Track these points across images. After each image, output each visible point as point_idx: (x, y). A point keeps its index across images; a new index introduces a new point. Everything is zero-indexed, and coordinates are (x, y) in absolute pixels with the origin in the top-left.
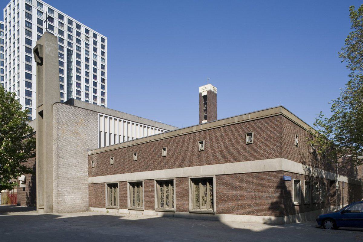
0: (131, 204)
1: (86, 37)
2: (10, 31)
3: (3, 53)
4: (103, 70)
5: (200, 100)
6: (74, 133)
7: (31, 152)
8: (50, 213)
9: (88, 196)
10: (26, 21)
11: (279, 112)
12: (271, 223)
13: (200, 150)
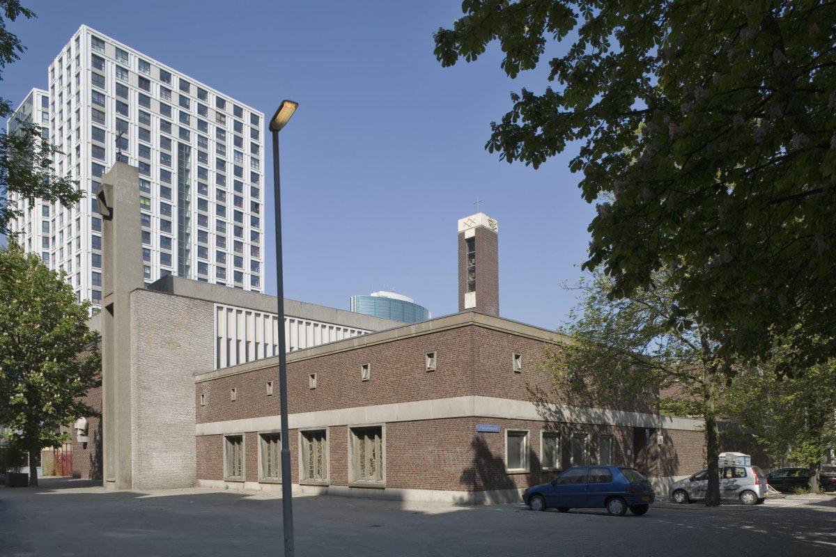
0: (264, 473)
1: (219, 116)
2: (61, 112)
3: (47, 220)
4: (255, 185)
5: (460, 248)
6: (169, 343)
7: (93, 378)
8: (125, 489)
9: (195, 459)
10: (93, 91)
11: (469, 320)
12: (461, 503)
13: (363, 380)
